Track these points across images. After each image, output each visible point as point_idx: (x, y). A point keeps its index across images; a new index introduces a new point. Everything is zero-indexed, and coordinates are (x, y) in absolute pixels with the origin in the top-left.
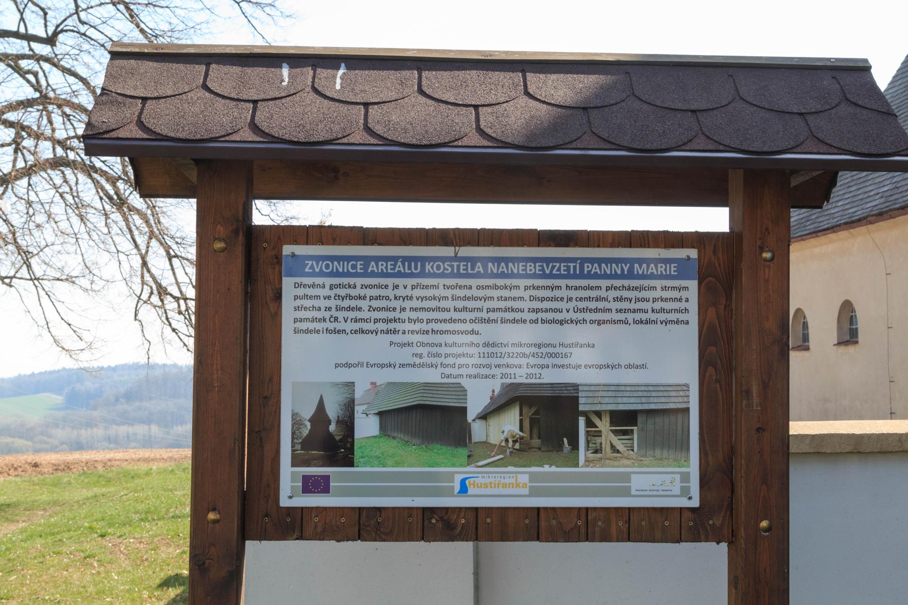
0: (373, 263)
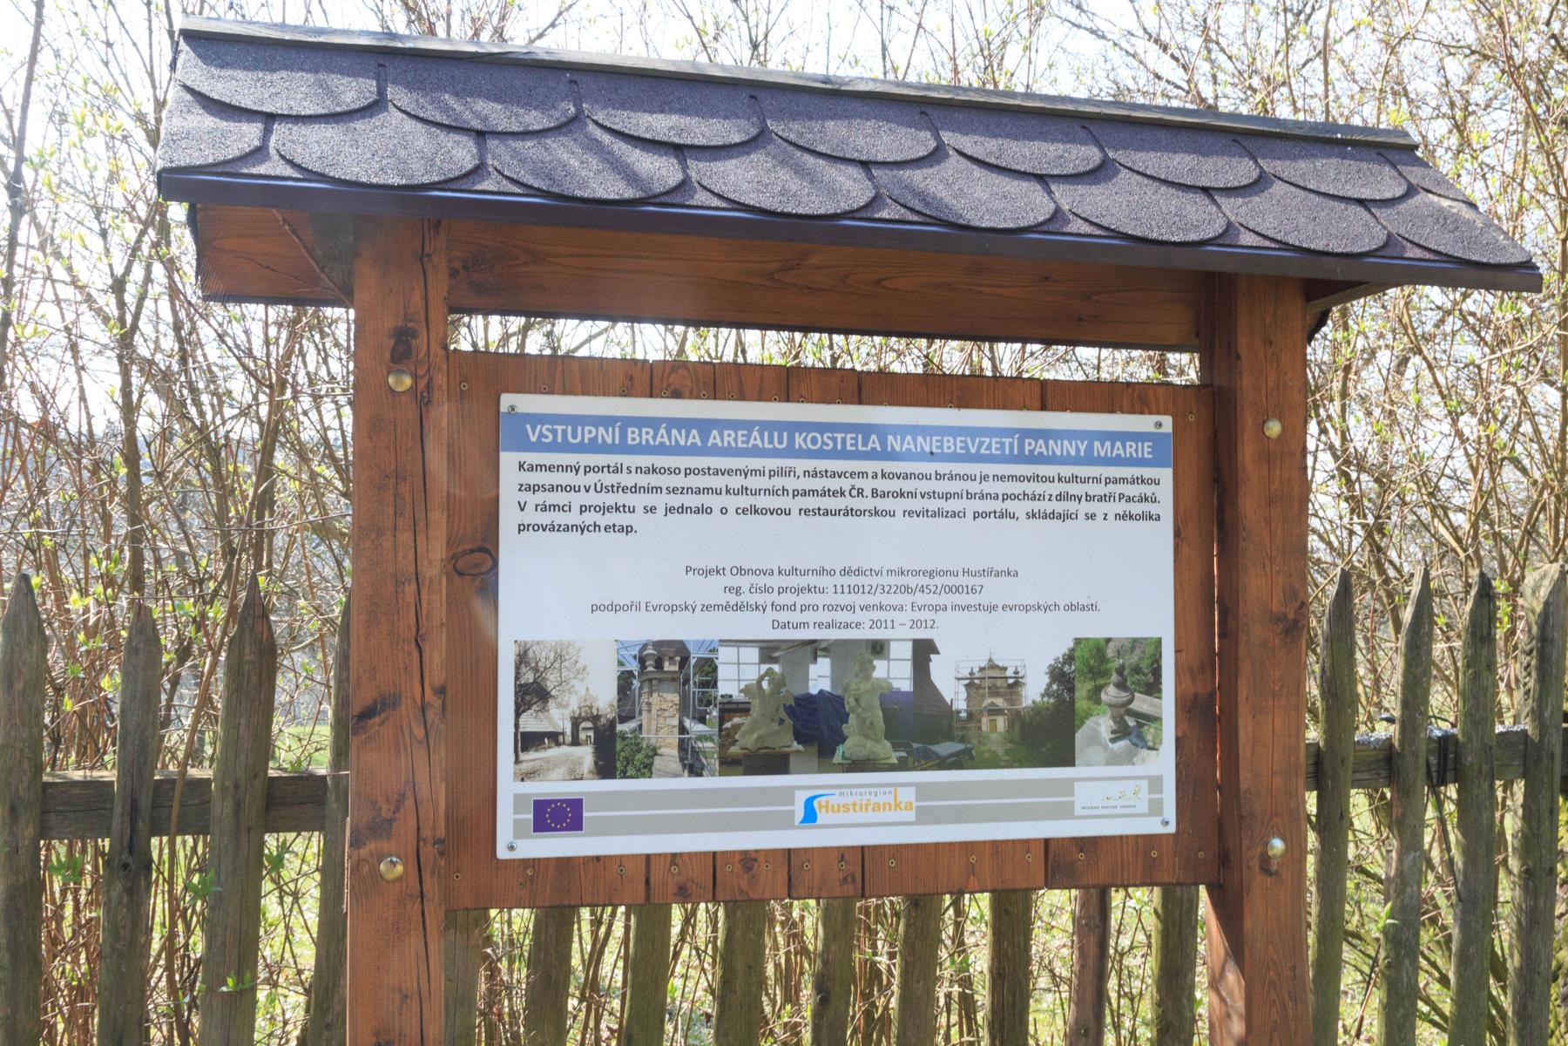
0: (715, 433)
